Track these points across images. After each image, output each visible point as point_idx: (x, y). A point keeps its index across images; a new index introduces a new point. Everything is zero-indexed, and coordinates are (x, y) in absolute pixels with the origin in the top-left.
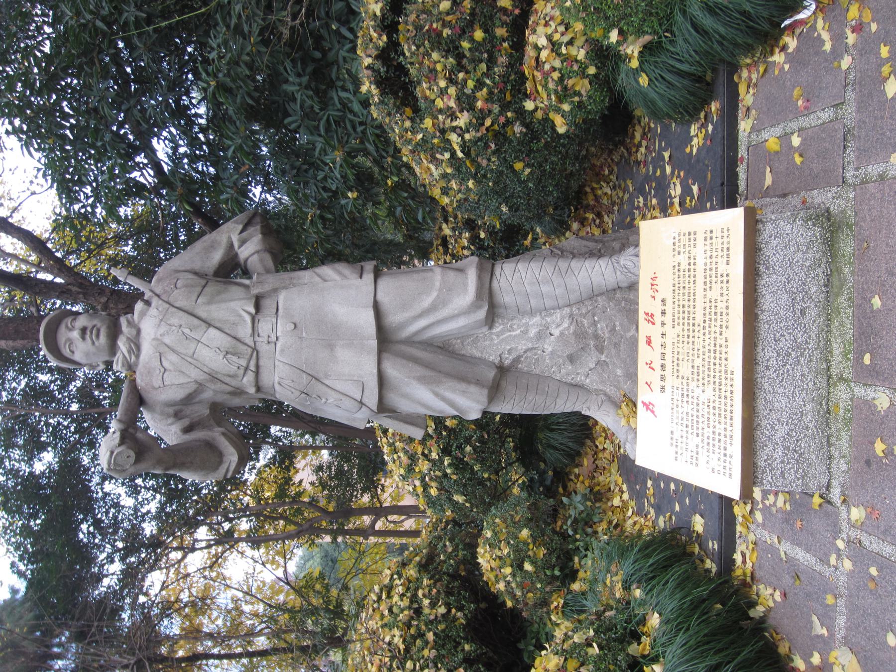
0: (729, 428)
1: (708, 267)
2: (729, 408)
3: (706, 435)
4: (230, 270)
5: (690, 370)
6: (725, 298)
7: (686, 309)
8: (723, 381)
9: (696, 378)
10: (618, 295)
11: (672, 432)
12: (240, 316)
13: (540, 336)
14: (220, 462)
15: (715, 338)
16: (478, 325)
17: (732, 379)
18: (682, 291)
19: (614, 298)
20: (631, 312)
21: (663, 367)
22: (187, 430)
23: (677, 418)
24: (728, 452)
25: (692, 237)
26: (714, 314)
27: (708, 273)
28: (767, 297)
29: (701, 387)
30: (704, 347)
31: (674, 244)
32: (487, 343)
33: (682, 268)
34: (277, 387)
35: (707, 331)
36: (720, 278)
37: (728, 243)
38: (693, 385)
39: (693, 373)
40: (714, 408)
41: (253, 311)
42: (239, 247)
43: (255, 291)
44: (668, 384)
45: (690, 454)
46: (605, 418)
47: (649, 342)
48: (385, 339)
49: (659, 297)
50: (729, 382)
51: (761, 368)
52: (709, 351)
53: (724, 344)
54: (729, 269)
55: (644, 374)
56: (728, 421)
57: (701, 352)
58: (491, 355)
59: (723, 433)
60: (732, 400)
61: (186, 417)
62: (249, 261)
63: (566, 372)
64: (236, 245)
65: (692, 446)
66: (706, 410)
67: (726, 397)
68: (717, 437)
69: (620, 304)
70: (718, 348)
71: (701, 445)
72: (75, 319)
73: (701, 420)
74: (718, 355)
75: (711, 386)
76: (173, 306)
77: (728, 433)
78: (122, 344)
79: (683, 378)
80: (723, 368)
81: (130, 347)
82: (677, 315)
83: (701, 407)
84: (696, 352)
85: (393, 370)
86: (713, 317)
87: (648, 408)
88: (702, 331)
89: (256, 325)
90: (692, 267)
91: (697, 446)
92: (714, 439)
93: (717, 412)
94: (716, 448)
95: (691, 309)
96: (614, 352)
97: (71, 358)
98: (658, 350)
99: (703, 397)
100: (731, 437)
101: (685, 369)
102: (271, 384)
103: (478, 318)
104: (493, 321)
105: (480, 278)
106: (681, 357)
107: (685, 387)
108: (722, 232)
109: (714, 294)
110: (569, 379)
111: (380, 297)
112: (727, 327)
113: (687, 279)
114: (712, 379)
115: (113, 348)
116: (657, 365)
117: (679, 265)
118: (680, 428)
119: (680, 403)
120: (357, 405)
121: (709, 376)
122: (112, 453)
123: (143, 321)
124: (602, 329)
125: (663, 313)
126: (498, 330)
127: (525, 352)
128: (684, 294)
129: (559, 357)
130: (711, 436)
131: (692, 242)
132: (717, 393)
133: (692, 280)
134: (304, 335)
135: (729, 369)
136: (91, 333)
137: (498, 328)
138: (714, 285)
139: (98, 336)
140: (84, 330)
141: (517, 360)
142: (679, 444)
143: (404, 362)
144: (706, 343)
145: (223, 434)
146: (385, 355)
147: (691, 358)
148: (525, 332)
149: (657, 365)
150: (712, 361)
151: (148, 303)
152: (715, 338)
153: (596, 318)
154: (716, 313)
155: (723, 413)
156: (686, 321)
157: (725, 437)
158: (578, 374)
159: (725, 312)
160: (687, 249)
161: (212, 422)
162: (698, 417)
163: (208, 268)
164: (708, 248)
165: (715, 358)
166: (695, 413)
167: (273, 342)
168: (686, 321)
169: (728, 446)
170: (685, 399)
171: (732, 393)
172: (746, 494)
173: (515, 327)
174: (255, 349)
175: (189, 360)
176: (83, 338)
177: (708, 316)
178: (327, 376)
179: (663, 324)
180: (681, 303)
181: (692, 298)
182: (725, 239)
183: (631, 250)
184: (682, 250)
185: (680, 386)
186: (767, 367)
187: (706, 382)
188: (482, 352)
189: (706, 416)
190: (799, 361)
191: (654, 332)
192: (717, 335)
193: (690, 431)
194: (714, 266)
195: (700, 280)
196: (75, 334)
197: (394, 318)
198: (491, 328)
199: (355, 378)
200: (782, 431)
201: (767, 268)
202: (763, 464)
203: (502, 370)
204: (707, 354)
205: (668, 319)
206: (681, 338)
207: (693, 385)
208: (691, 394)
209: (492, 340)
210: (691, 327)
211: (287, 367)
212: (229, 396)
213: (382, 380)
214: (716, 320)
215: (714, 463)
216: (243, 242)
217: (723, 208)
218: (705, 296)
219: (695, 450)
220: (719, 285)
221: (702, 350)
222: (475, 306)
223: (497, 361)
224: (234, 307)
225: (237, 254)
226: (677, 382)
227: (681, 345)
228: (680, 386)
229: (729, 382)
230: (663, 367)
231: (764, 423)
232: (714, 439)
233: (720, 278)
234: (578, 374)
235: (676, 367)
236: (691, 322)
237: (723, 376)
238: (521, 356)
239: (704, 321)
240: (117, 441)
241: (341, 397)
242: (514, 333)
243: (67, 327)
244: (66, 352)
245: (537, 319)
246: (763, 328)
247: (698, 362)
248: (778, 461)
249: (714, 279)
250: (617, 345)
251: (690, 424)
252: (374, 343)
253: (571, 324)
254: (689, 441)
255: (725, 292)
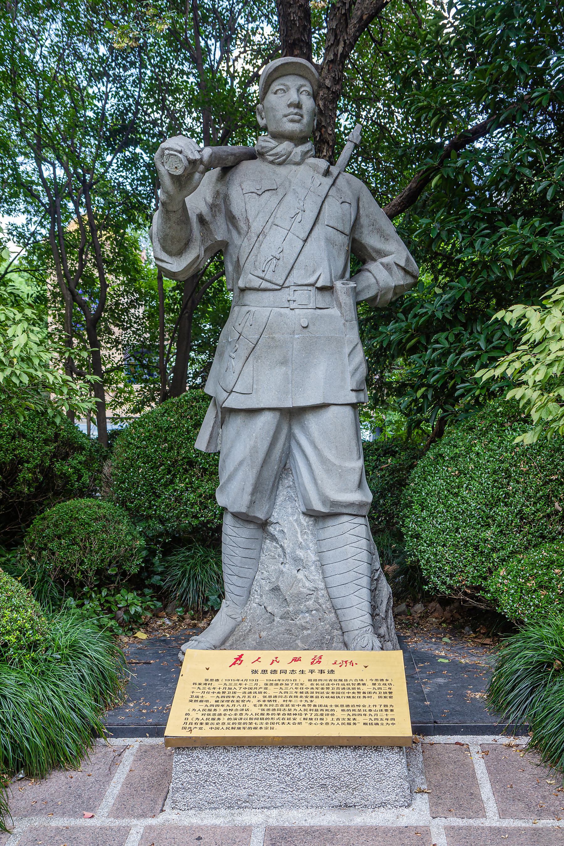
0: (225, 727)
1: (361, 708)
2: (242, 726)
3: (217, 708)
4: (358, 257)
5: (273, 695)
6: (336, 722)
7: (325, 691)
8: (265, 721)
9: (266, 699)
10: (337, 633)
11: (218, 680)
12: (314, 272)
13: (297, 560)
14: (170, 254)
15: (301, 714)
16: (306, 501)
17: (266, 728)
18: (341, 687)
19: (333, 628)
20: (323, 643)
21: (275, 672)
22: (201, 219)
23: (230, 684)
24: (204, 726)
25: (388, 695)
26: (323, 713)
27: (357, 708)
28: (336, 757)
29: (258, 704)
30: (293, 706)
31: (382, 680)
32: (290, 510)
33: (361, 687)
34: (246, 309)
35: (307, 707)
36: (352, 717)
37: (382, 724)
38: (260, 697)
39: (270, 697)
40: (241, 714)
41: (319, 285)
42: (382, 264)
43: (338, 284)
44: (259, 676)
45: (200, 695)
46: (221, 623)
47: (295, 660)
48: (293, 415)
49: (336, 668)
50: (264, 726)
51: (276, 752)
52: (290, 710)
53: (296, 722)
54: (360, 726)
55: (267, 655)
56: (231, 726)
57: (288, 703)
58: (278, 514)
59: (220, 722)
60: (249, 728)
61: (214, 216)
62: (369, 274)
63: (262, 584)
64: (385, 260)
65: (207, 697)
66: (239, 708)
67: (251, 724)
68: (217, 717)
69: (329, 634)
70: (292, 717)
71: (208, 704)
72: (309, 95)
73: (230, 704)
74: (286, 717)
75: (260, 712)
76: (323, 202)
77: (221, 726)
78: (286, 146)
79: (266, 688)
80: (275, 721)
81: (282, 156)
82: (320, 683)
83: (242, 704)
84: (288, 699)
85: (266, 422)
86: (319, 713)
87: (237, 659)
88: (306, 704)
89: (306, 288)
90: (362, 695)
91: (207, 701)
92: (214, 714)
93: (238, 717)
94: (206, 717)
95: (325, 695)
96: (282, 629)
97: (270, 91)
98: (289, 668)
99: (250, 705)
100: (218, 728)
101: (272, 691)
102: (248, 303)
103: (314, 503)
104: (311, 516)
105: (352, 505)
106: (283, 687)
107: (257, 691)
108: (392, 719)
109: (338, 713)
110: (255, 587)
111: (332, 408)
112: (311, 724)
113: (352, 691)
114: (266, 712)
115: (279, 136)
116: (275, 666)
117: (364, 684)
118: (222, 687)
119: (244, 686)
120: (229, 388)
121: (268, 710)
122: (181, 152)
123: (308, 167)
124: (304, 618)
125: (322, 672)
126: (302, 521)
127: (281, 546)
128: (338, 688)
129: (278, 578)
130: (217, 713)
131: (383, 695)
132: (254, 717)
133: (351, 695)
134: (296, 336)
135: (275, 726)
136: (296, 114)
137: (304, 520)
138: (346, 713)
139: (292, 121)
140: (298, 106)
141: (273, 538)
142: (207, 686)
143: (272, 433)
144: (296, 707)
145: (198, 257)
146: (278, 414)
147: (284, 695)
148: (300, 546)
149: (275, 666)
150: (282, 712)
151: (327, 173)
152: (301, 714)
153: (314, 612)
154: (322, 715)
155: (237, 721)
156: (315, 690)
157: (218, 724)
158: (261, 596)
159: (324, 722)
160: (377, 691)
161: (210, 243)
162: (233, 701)
163: (362, 233)
164: (378, 708)
165: (284, 714)
166: (235, 699)
167: (290, 304)
168: (315, 690)
169: (210, 726)
170: (247, 691)
171: (255, 728)
172: (169, 741)
173: (305, 537)
174: (282, 287)
175: (270, 221)
176: (290, 106)
177: (319, 708)
178: (258, 358)
179: (312, 672)
180: (331, 686)
181: (335, 695)
182: (385, 722)
183: (377, 643)
184: (376, 687)
185: (258, 687)
186: (277, 757)
187: (263, 707)
188: (280, 505)
189: (234, 708)
190: (282, 783)
191: (305, 665)
192: (304, 716)
193: (220, 695)
194: (362, 713)
195: (351, 702)
196: (293, 96)
197: (313, 422)
198: (304, 513)
199: (255, 386)
200: (223, 770)
201: (360, 756)
202: (195, 755)
203: (263, 525)
204: (287, 708)
205: (316, 676)
206: (300, 686)
207: (260, 697)
208: (252, 695)
209: (293, 515)
210: (309, 695)
211: (265, 320)
212: (235, 259)
213: (253, 412)
214: (316, 715)
215: (193, 715)
216: (387, 267)
217: (412, 723)
218: (337, 706)
219: (204, 699)
220: (346, 717)
221: (290, 704)
222: (325, 500)
223: (272, 519)
224: (322, 260)
225: (374, 260)
226: (261, 684)
227: (294, 686)
228: (258, 687)
229: (264, 726)
230: (275, 672)
231: (230, 755)
232: (214, 714)
233: (352, 717)
234: (261, 596)
235: (274, 682)
236: (315, 695)
237: (269, 721)
238: (277, 543)
239: (315, 706)
240: (191, 157)
241: (237, 373)
242: (299, 535)
243: (302, 86)
244: (275, 86)
245: (313, 557)
246: (311, 754)
247: (280, 701)
248: (198, 767)
249: (351, 713)
250: (289, 632)
251: (226, 695)
252: (289, 404)
253: (309, 589)
254: (211, 695)
255: (340, 722)
